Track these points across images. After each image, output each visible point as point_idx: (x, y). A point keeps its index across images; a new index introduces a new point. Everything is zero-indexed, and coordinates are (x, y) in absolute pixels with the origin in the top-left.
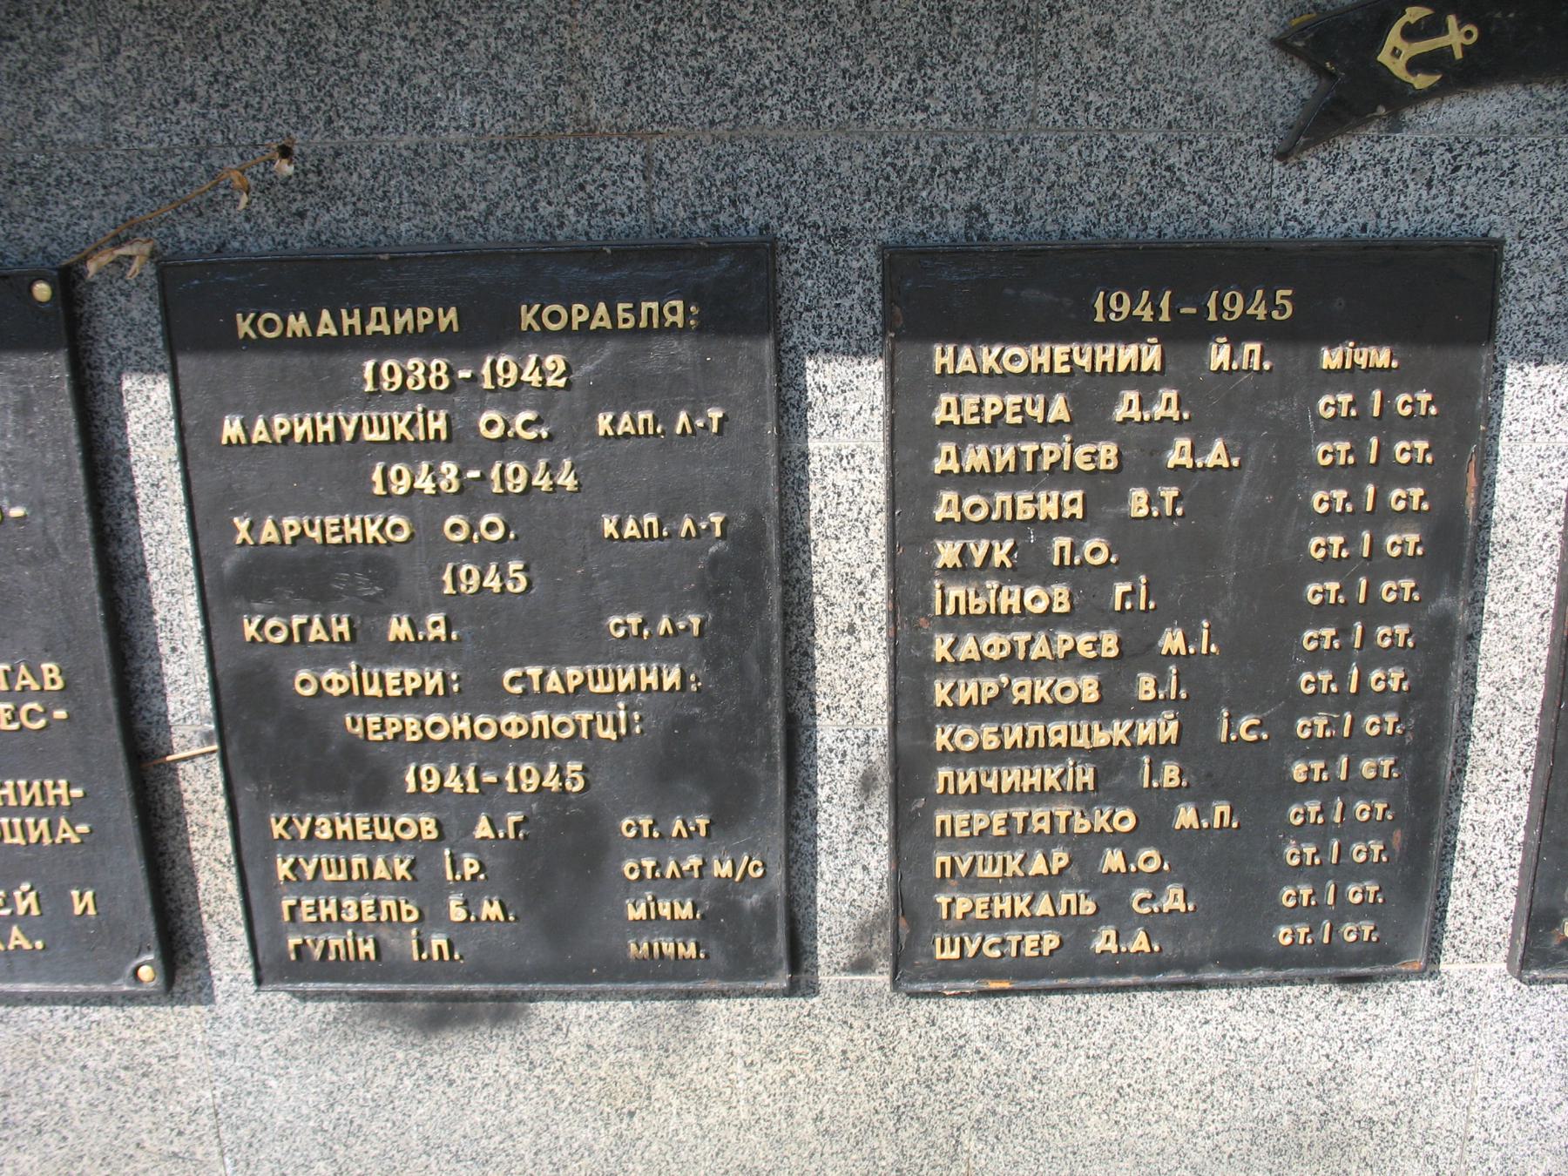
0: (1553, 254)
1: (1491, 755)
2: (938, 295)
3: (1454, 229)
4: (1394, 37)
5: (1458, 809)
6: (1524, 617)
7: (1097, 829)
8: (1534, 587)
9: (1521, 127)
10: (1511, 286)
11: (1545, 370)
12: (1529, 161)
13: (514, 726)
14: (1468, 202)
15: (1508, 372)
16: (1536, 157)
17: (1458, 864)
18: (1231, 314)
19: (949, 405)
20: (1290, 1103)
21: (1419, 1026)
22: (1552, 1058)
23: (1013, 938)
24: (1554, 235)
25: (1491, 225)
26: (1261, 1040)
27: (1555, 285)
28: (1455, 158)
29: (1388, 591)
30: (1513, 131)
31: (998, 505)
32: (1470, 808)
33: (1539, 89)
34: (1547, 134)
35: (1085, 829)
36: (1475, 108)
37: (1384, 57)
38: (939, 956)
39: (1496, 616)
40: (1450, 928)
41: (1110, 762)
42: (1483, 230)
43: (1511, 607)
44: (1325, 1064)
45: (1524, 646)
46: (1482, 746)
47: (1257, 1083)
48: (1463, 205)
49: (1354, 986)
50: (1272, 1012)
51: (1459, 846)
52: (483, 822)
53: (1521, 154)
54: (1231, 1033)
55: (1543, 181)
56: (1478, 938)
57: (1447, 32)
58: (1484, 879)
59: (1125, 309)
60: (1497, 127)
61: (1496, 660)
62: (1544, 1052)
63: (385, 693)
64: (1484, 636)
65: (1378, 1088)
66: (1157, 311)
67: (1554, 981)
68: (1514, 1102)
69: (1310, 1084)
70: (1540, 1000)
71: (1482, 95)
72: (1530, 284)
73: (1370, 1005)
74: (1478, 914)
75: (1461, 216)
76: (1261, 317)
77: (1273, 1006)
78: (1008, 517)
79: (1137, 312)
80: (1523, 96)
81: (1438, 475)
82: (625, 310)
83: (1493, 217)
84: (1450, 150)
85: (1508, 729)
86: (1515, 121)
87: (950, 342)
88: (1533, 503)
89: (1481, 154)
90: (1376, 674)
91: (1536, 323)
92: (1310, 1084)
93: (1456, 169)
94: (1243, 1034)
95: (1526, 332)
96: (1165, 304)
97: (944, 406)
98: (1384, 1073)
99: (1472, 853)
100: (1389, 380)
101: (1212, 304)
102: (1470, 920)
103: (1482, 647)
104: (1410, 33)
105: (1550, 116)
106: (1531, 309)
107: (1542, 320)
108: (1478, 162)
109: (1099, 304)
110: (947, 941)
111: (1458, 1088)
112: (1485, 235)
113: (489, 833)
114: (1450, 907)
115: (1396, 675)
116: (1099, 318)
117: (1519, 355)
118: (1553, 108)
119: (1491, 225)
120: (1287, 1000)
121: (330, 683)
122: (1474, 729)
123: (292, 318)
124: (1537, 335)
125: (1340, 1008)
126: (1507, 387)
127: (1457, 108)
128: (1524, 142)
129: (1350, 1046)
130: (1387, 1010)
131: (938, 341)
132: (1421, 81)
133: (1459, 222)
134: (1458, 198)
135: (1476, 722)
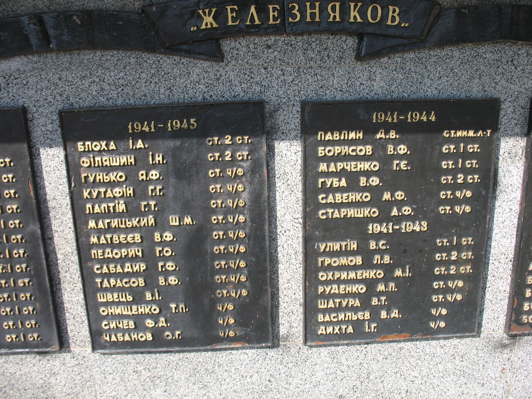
0: (47, 111)
1: (68, 278)
3: (12, 104)
5: (62, 296)
6: (67, 232)
8: (67, 221)
9: (27, 69)
10: (35, 122)
11: (53, 149)
12: (32, 80)
14: (15, 95)
15: (41, 150)
16: (34, 79)
17: (67, 314)
18: (177, 127)
20: (33, 394)
21: (69, 369)
22: (119, 379)
24: (46, 104)
25: (24, 102)
26: (17, 373)
27: (50, 121)
28: (7, 81)
30: (25, 71)
32: (66, 296)
33: (30, 57)
34: (36, 71)
36: (10, 64)
39: (57, 231)
40: (70, 336)
42: (21, 104)
43: (62, 229)
44: (42, 382)
45: (70, 241)
46: (64, 275)
47: (20, 388)
48: (13, 96)
49: (43, 355)
50: (18, 363)
51: (66, 309)
53: (29, 78)
54: (6, 371)
55: (38, 87)
56: (81, 339)
58: (78, 320)
59: (383, 118)
60: (19, 70)
61: (61, 246)
62: (116, 378)
64: (55, 238)
65: (62, 390)
66: (393, 119)
67: (112, 354)
68: (111, 395)
69: (38, 388)
70: (109, 360)
71: (11, 60)
72: (42, 121)
73: (51, 362)
74: (79, 331)
75: (13, 100)
76: (425, 120)
77: (18, 362)
78: (91, 212)
79: (143, 129)
80: (25, 59)
81: (19, 186)
83: (24, 99)
84: (5, 78)
85: (72, 269)
86: (24, 68)
87: (103, 140)
88: (60, 194)
89: (15, 79)
91: (47, 134)
92: (38, 388)
93: (8, 84)
94: (10, 371)
95: (44, 137)
96: (395, 117)
98: (63, 384)
99: (71, 311)
101: (409, 116)
102: (76, 333)
103: (55, 242)
105: (36, 65)
106: (44, 129)
107: (48, 133)
108: (15, 82)
111: (90, 390)
112: (23, 106)
114: (68, 329)
116: (374, 121)
117: (44, 145)
118: (36, 63)
119: (24, 102)
120: (22, 359)
122: (60, 269)
124: (48, 138)
125: (41, 362)
126: (41, 156)
127: (4, 64)
128: (29, 75)
129: (48, 375)
130: (57, 363)
131: (80, 140)
133: (13, 102)
134: (11, 94)
135: (60, 267)
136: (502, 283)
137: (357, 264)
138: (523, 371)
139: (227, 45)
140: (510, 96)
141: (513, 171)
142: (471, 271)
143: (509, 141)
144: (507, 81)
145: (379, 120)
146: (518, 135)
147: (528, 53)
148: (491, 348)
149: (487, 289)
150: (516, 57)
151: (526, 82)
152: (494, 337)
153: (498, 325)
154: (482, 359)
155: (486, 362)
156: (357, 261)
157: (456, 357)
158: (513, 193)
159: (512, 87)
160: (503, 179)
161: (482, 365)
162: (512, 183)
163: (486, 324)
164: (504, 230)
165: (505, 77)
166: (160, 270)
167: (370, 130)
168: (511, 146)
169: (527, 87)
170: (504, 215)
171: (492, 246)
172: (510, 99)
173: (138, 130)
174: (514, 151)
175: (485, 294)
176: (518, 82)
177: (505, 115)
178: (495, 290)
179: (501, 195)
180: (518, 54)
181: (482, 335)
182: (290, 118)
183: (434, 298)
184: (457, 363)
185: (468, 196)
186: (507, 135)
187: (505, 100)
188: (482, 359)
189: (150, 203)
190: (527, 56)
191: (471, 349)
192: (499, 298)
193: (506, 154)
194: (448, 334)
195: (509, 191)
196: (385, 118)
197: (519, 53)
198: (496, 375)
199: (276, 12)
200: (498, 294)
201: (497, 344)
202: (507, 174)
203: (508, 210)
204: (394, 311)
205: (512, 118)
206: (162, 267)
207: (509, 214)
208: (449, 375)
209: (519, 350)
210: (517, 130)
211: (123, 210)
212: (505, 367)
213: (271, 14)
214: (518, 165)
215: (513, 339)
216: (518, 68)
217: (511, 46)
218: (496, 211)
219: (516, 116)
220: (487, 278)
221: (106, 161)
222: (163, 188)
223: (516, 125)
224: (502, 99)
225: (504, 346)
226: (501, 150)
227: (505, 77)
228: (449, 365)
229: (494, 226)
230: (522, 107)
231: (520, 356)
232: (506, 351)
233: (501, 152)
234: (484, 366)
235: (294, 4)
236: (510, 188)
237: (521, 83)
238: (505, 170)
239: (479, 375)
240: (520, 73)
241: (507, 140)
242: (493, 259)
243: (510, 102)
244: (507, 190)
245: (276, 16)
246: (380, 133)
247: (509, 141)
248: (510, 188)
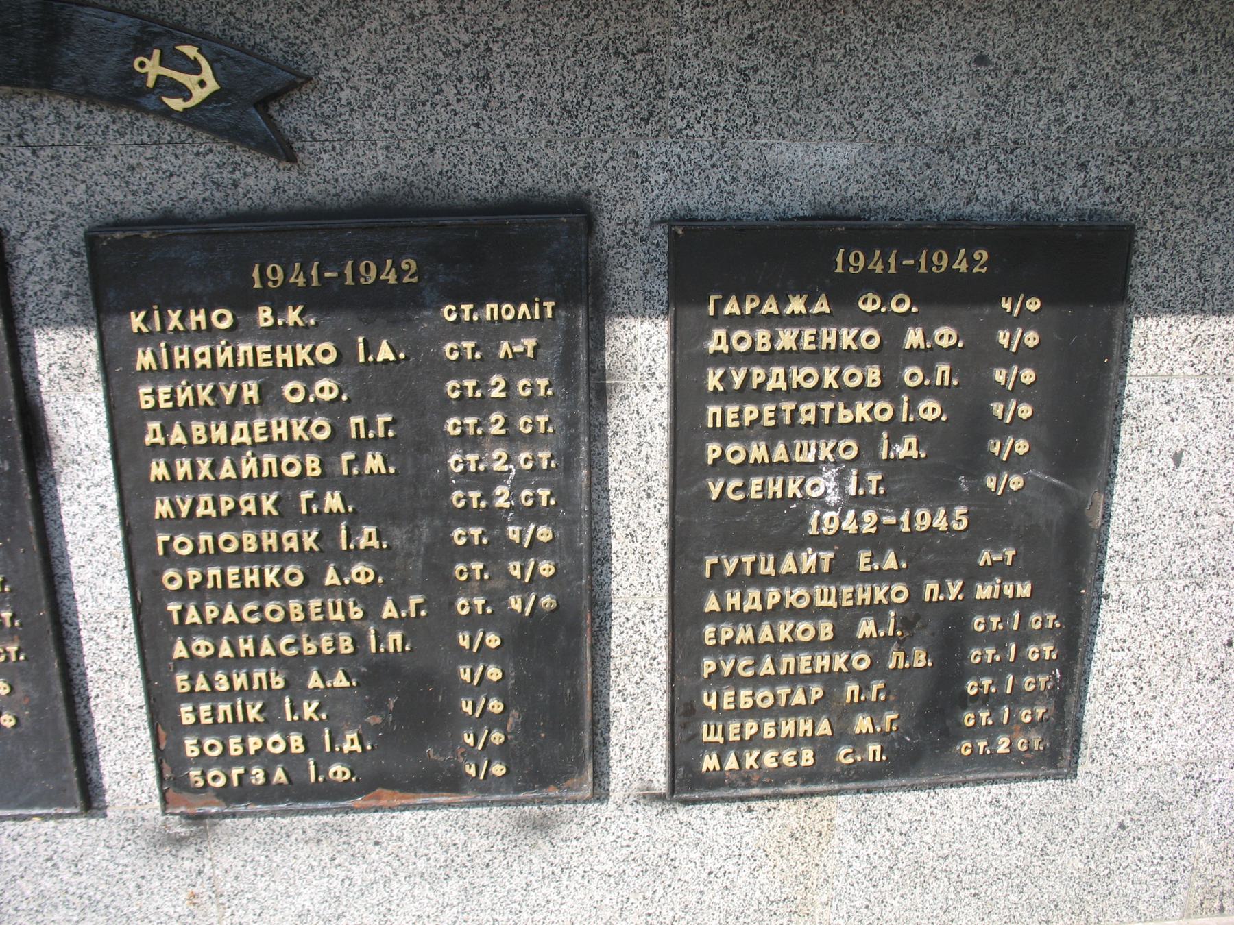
2: (715, 261)
4: (199, 95)
7: (858, 420)
13: (363, 574)
19: (720, 338)
29: (1032, 653)
35: (849, 419)
37: (212, 85)
38: (705, 739)
41: (845, 619)
52: (331, 572)
57: (159, 76)
63: (253, 440)
66: (886, 265)
90: (1035, 617)
96: (892, 260)
100: (1026, 606)
104: (185, 93)
109: (839, 259)
110: (712, 727)
113: (337, 581)
115: (1047, 648)
116: (839, 270)
121: (198, 648)
136: (128, 689)
138: (245, 901)
140: (34, 225)
141: (85, 411)
142: (1058, 625)
143: (56, 337)
144: (19, 187)
145: (851, 270)
146: (76, 321)
147: (58, 115)
148: (144, 845)
149: (92, 703)
150: (30, 126)
151: (70, 188)
152: (143, 819)
153: (146, 790)
154: (129, 869)
155: (143, 877)
157: (61, 865)
158: (98, 467)
159: (35, 200)
160: (62, 432)
161: (134, 884)
162: (88, 442)
163: (115, 787)
164: (98, 558)
165: (11, 176)
167: (844, 294)
168: (64, 349)
169: (75, 201)
170: (88, 521)
171: (77, 597)
172: (37, 232)
173: (275, 282)
174: (74, 361)
175: (89, 712)
176: (47, 188)
177: (30, 273)
178: (116, 704)
179: (66, 470)
180: (33, 118)
181: (110, 812)
182: (636, 266)
183: (971, 688)
184: (66, 878)
185: (1021, 451)
186: (47, 322)
187: (23, 234)
188: (129, 869)
189: (540, 455)
190: (58, 123)
191: (94, 846)
192: (131, 724)
193: (56, 370)
194: (8, 808)
195: (85, 462)
196: (378, 275)
197: (35, 114)
198: (178, 909)
200: (126, 715)
201: (158, 836)
202: (70, 419)
203: (97, 509)
204: (349, 737)
205: (51, 279)
207: (101, 518)
208: (56, 907)
209: (218, 850)
210: (71, 308)
211: (186, 475)
212: (195, 890)
214: (93, 396)
215: (198, 825)
216: (42, 153)
217: (11, 98)
218: (64, 510)
219: (61, 275)
220: (85, 674)
221: (203, 355)
222: (394, 421)
223: (66, 298)
224: (13, 233)
225: (178, 840)
226: (39, 360)
227: (11, 176)
228: (47, 883)
229: (70, 548)
230: (72, 252)
231: (227, 866)
232: (187, 852)
233: (42, 364)
234: (138, 886)
236: (86, 453)
237: (57, 190)
238: (62, 410)
239: (135, 908)
240: (47, 165)
241: (51, 334)
242: (88, 627)
243: (37, 239)
244: (80, 459)
246: (818, 304)
247: (56, 337)
248: (86, 453)
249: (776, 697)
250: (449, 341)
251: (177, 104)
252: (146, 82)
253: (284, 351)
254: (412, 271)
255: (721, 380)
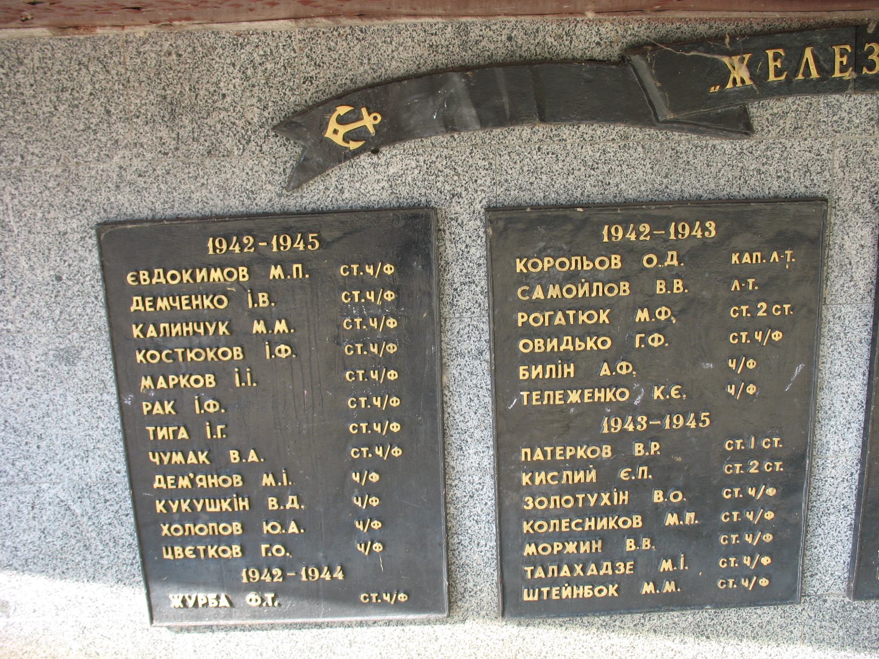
4: (333, 125)
23: (545, 590)
31: (162, 330)
37: (329, 134)
57: (363, 119)
82: (312, 238)
97: (135, 303)
101: (672, 230)
104: (341, 121)
123: (213, 271)
132: (353, 145)
137: (235, 533)
139: (760, 112)
156: (235, 529)
166: (264, 554)
199: (779, 60)
206: (267, 550)
213: (771, 64)
235: (872, 45)
245: (845, 63)
249: (576, 500)
250: (720, 513)
251: (342, 110)
252: (368, 109)
253: (599, 398)
254: (250, 245)
255: (164, 506)
